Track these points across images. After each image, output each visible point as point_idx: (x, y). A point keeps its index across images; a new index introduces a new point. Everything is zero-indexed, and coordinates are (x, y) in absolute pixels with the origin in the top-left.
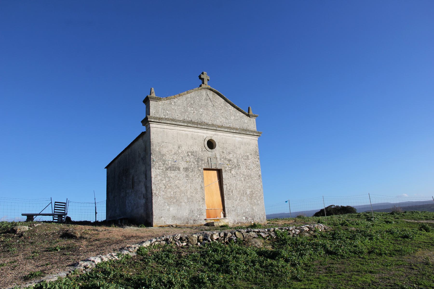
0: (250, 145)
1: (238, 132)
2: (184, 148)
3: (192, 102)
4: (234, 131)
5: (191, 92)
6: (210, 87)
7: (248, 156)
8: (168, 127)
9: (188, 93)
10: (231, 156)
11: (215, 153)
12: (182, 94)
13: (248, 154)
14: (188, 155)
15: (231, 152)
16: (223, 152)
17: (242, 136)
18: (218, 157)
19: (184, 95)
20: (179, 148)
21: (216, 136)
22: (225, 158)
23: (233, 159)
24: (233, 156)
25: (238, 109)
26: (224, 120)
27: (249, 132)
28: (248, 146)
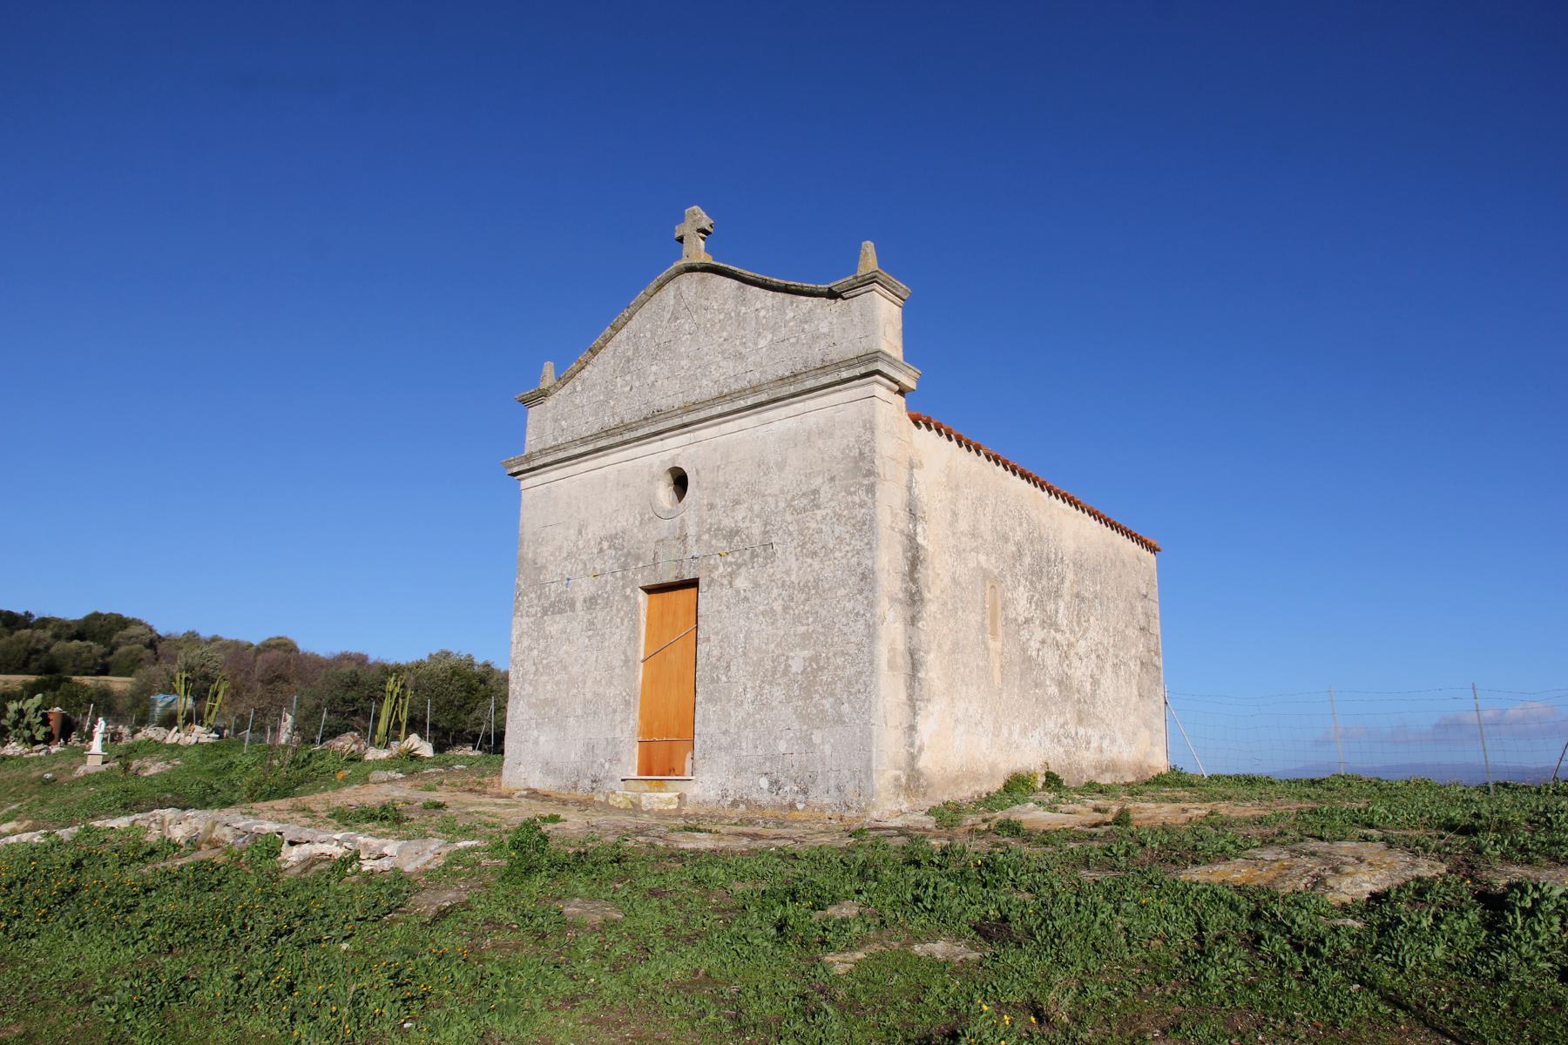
0: (831, 435)
1: (763, 397)
2: (594, 531)
3: (630, 353)
4: (750, 402)
5: (630, 318)
6: (708, 260)
7: (816, 492)
8: (569, 470)
9: (617, 330)
10: (741, 512)
11: (683, 520)
12: (599, 340)
13: (817, 482)
14: (601, 550)
15: (744, 497)
16: (711, 506)
17: (799, 406)
18: (692, 531)
19: (607, 340)
20: (580, 532)
21: (692, 449)
22: (718, 529)
23: (747, 523)
24: (751, 509)
25: (786, 290)
26: (729, 367)
27: (815, 377)
28: (820, 443)
